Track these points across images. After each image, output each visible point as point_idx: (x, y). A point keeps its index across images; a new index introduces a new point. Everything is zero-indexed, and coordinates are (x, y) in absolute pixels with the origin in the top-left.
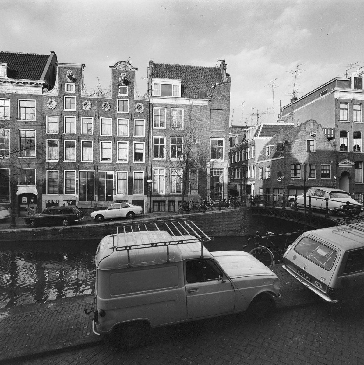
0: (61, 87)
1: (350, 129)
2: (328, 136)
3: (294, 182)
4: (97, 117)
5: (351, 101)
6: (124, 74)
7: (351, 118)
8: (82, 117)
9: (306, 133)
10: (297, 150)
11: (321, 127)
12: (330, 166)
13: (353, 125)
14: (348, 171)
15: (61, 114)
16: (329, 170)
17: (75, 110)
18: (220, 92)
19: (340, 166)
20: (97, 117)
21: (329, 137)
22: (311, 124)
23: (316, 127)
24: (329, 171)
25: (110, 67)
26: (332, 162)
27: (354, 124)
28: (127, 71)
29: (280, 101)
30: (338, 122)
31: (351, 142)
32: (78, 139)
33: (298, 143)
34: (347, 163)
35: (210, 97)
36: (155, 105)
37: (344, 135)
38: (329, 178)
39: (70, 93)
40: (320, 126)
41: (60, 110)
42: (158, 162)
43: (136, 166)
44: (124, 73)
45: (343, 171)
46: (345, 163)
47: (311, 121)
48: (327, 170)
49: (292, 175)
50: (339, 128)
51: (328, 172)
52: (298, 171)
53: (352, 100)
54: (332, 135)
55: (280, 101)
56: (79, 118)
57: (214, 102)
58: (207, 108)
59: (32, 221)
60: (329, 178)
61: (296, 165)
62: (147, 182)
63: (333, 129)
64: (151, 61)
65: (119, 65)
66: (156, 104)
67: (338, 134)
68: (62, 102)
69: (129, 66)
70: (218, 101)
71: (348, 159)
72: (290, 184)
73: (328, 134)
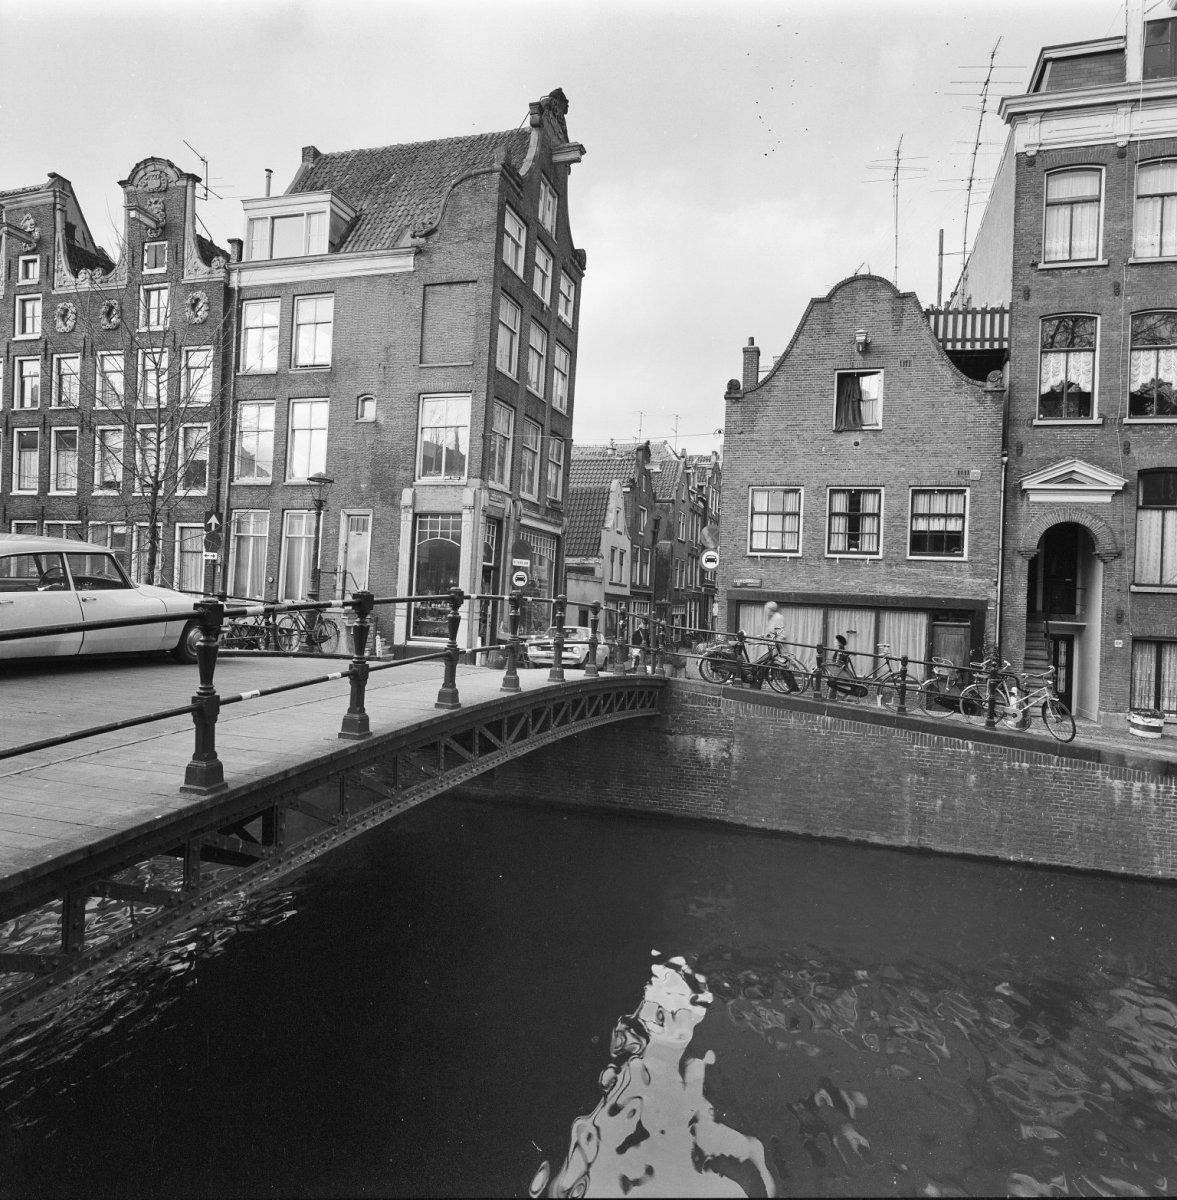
0: (9, 269)
1: (1106, 301)
2: (954, 346)
3: (763, 573)
4: (88, 352)
5: (1122, 153)
6: (156, 202)
7: (1119, 237)
8: (56, 356)
9: (834, 340)
10: (782, 426)
11: (917, 304)
12: (968, 494)
13: (1127, 278)
14: (1085, 520)
15: (8, 352)
16: (962, 516)
17: (37, 336)
18: (460, 215)
19: (1033, 498)
20: (88, 352)
21: (963, 352)
22: (862, 296)
23: (887, 306)
24: (960, 522)
25: (120, 183)
26: (975, 473)
27: (1136, 270)
28: (165, 191)
29: (942, 231)
30: (1028, 270)
31: (1114, 368)
32: (44, 423)
33: (787, 390)
34: (1075, 476)
35: (423, 240)
36: (246, 294)
37: (1069, 332)
38: (962, 555)
39: (29, 285)
40: (909, 305)
41: (6, 340)
42: (246, 491)
43: (185, 505)
44: (156, 199)
45: (1051, 520)
46: (1069, 478)
47: (858, 285)
48: (947, 516)
49: (839, 543)
50: (1033, 302)
51: (953, 526)
52: (868, 525)
53: (1122, 142)
54: (973, 340)
55: (942, 231)
56: (46, 359)
57: (435, 258)
58: (413, 283)
59: (1111, 644)
60: (962, 555)
61: (859, 492)
62: (216, 554)
63: (1002, 311)
64: (306, 148)
65: (141, 173)
66: (249, 288)
67: (1033, 333)
68: (11, 315)
69: (169, 171)
70: (451, 248)
71: (1076, 455)
72: (739, 582)
73: (954, 340)
